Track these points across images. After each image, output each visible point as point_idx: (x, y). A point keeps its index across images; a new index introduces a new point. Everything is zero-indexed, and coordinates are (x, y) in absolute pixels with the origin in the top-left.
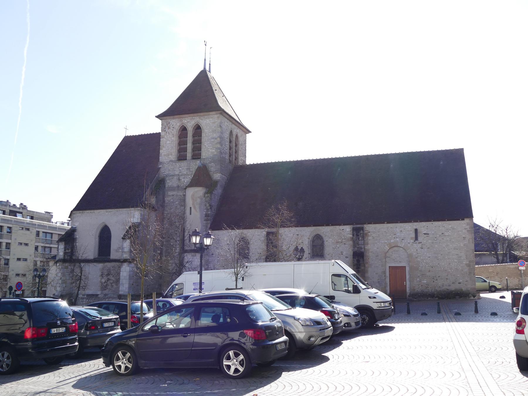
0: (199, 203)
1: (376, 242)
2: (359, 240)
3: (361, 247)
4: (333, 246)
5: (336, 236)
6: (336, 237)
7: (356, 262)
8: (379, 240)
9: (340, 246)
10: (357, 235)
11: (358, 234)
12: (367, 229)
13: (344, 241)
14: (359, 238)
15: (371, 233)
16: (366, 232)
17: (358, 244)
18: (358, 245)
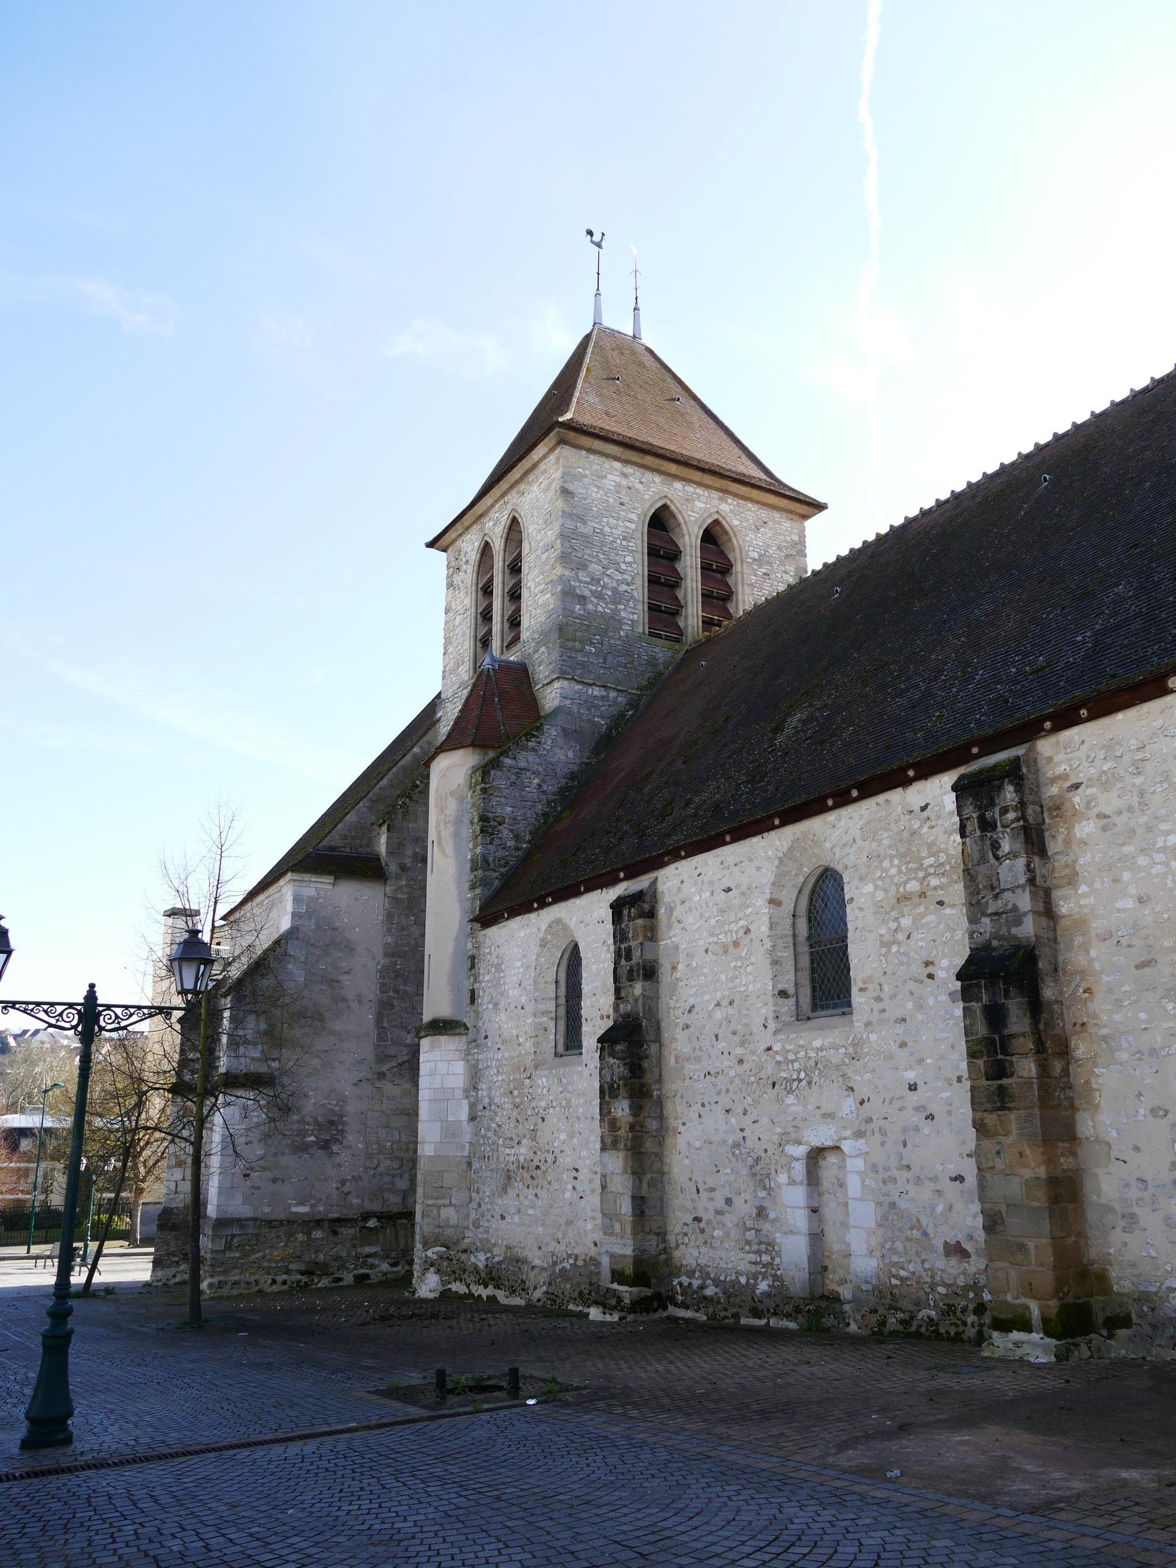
0: (452, 818)
1: (1129, 849)
2: (997, 858)
3: (1015, 908)
4: (883, 931)
5: (892, 857)
6: (892, 865)
7: (981, 1029)
8: (1149, 829)
9: (914, 920)
10: (987, 825)
11: (988, 814)
12: (1060, 770)
13: (934, 882)
14: (995, 846)
15: (1089, 791)
16: (1054, 790)
17: (996, 890)
18: (996, 897)
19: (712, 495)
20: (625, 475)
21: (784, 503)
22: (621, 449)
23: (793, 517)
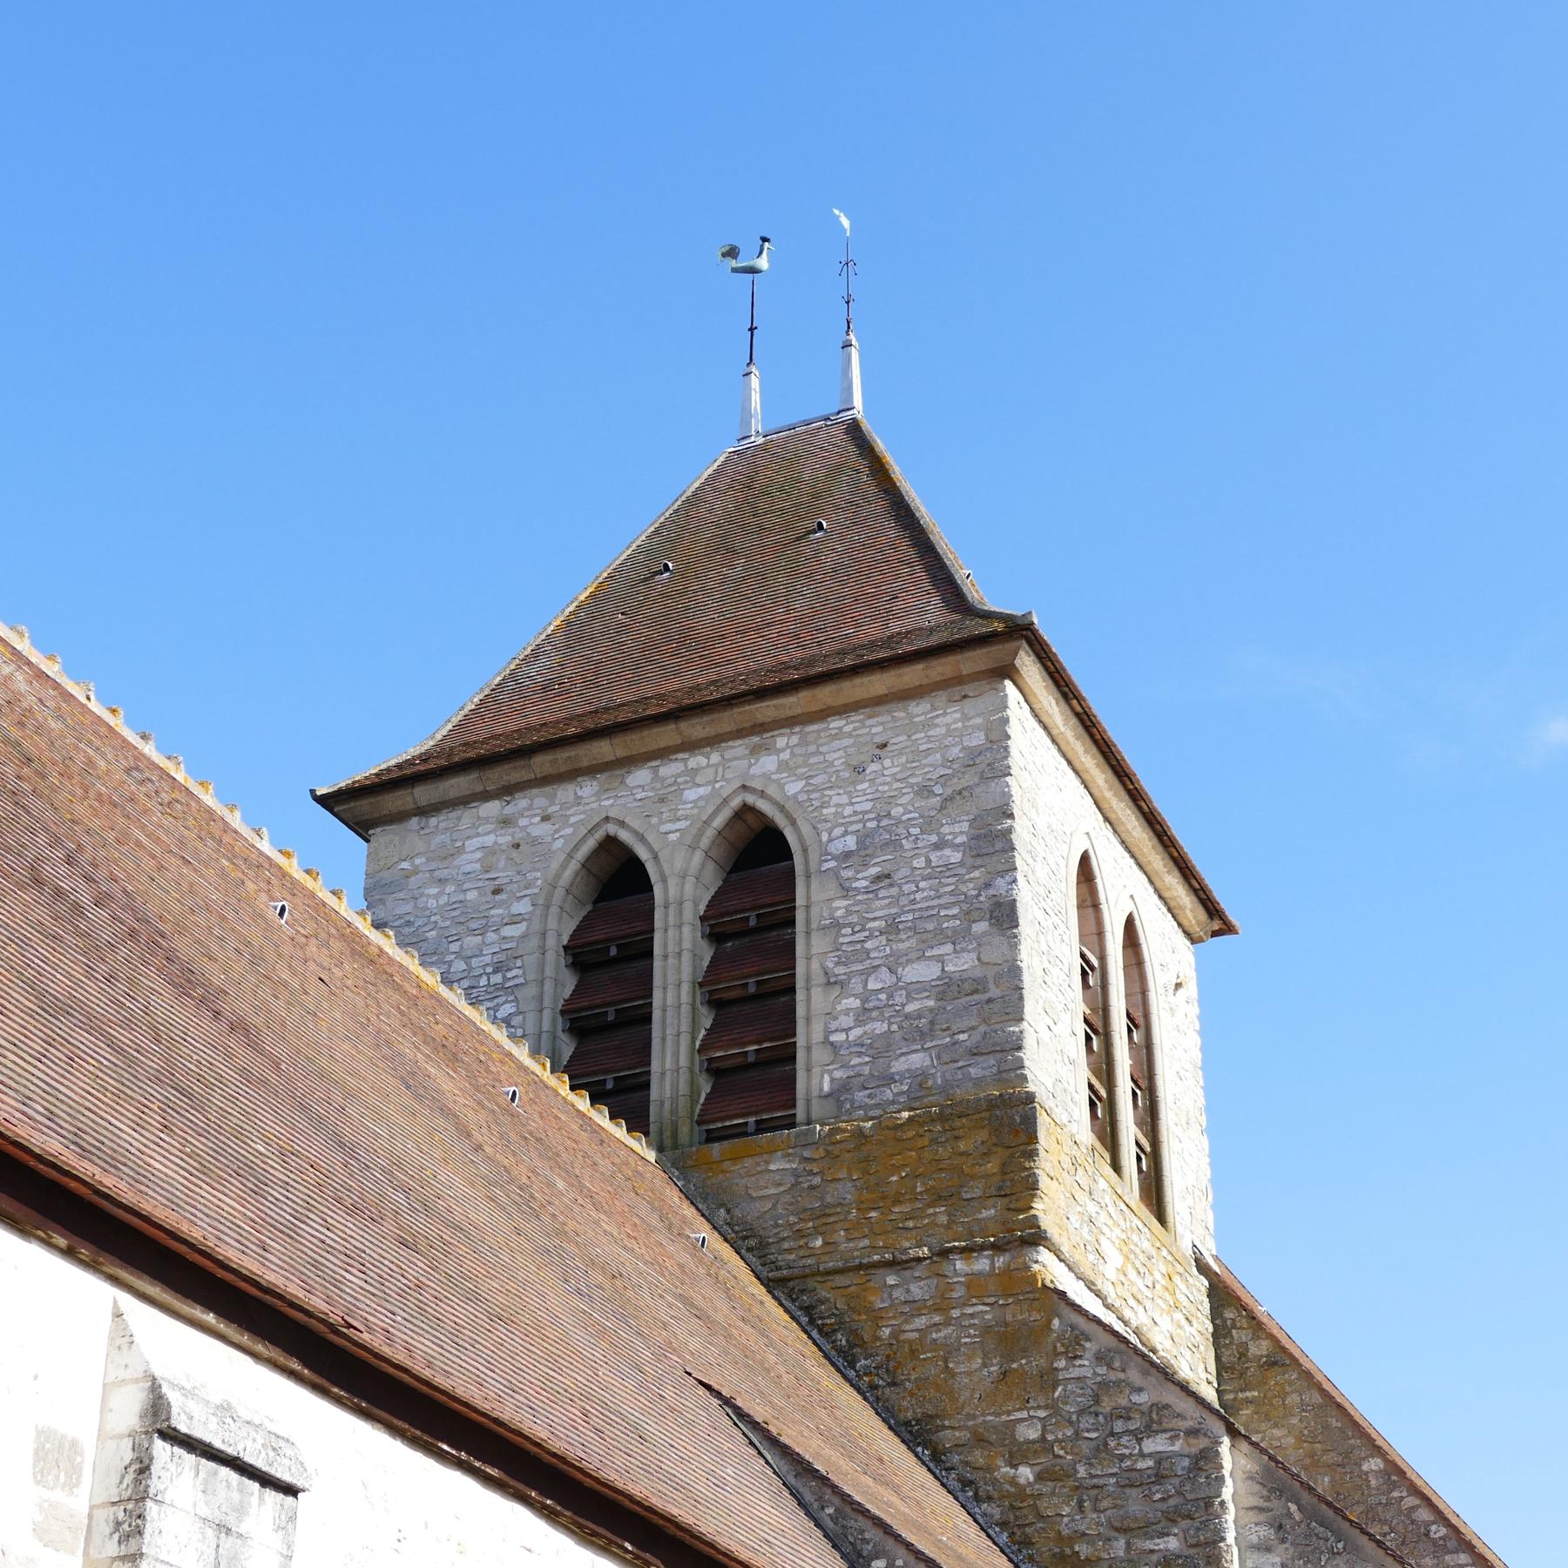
19: (729, 754)
20: (506, 822)
21: (912, 675)
22: (474, 776)
23: (968, 689)
